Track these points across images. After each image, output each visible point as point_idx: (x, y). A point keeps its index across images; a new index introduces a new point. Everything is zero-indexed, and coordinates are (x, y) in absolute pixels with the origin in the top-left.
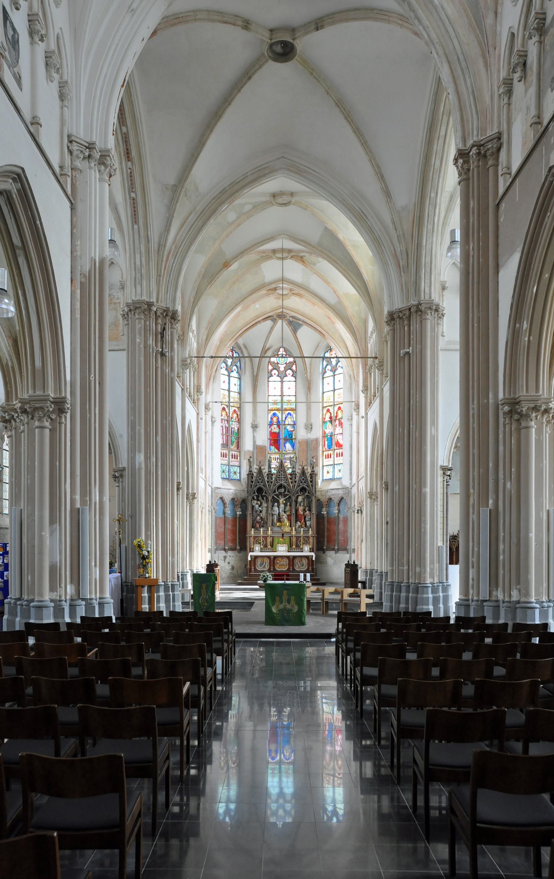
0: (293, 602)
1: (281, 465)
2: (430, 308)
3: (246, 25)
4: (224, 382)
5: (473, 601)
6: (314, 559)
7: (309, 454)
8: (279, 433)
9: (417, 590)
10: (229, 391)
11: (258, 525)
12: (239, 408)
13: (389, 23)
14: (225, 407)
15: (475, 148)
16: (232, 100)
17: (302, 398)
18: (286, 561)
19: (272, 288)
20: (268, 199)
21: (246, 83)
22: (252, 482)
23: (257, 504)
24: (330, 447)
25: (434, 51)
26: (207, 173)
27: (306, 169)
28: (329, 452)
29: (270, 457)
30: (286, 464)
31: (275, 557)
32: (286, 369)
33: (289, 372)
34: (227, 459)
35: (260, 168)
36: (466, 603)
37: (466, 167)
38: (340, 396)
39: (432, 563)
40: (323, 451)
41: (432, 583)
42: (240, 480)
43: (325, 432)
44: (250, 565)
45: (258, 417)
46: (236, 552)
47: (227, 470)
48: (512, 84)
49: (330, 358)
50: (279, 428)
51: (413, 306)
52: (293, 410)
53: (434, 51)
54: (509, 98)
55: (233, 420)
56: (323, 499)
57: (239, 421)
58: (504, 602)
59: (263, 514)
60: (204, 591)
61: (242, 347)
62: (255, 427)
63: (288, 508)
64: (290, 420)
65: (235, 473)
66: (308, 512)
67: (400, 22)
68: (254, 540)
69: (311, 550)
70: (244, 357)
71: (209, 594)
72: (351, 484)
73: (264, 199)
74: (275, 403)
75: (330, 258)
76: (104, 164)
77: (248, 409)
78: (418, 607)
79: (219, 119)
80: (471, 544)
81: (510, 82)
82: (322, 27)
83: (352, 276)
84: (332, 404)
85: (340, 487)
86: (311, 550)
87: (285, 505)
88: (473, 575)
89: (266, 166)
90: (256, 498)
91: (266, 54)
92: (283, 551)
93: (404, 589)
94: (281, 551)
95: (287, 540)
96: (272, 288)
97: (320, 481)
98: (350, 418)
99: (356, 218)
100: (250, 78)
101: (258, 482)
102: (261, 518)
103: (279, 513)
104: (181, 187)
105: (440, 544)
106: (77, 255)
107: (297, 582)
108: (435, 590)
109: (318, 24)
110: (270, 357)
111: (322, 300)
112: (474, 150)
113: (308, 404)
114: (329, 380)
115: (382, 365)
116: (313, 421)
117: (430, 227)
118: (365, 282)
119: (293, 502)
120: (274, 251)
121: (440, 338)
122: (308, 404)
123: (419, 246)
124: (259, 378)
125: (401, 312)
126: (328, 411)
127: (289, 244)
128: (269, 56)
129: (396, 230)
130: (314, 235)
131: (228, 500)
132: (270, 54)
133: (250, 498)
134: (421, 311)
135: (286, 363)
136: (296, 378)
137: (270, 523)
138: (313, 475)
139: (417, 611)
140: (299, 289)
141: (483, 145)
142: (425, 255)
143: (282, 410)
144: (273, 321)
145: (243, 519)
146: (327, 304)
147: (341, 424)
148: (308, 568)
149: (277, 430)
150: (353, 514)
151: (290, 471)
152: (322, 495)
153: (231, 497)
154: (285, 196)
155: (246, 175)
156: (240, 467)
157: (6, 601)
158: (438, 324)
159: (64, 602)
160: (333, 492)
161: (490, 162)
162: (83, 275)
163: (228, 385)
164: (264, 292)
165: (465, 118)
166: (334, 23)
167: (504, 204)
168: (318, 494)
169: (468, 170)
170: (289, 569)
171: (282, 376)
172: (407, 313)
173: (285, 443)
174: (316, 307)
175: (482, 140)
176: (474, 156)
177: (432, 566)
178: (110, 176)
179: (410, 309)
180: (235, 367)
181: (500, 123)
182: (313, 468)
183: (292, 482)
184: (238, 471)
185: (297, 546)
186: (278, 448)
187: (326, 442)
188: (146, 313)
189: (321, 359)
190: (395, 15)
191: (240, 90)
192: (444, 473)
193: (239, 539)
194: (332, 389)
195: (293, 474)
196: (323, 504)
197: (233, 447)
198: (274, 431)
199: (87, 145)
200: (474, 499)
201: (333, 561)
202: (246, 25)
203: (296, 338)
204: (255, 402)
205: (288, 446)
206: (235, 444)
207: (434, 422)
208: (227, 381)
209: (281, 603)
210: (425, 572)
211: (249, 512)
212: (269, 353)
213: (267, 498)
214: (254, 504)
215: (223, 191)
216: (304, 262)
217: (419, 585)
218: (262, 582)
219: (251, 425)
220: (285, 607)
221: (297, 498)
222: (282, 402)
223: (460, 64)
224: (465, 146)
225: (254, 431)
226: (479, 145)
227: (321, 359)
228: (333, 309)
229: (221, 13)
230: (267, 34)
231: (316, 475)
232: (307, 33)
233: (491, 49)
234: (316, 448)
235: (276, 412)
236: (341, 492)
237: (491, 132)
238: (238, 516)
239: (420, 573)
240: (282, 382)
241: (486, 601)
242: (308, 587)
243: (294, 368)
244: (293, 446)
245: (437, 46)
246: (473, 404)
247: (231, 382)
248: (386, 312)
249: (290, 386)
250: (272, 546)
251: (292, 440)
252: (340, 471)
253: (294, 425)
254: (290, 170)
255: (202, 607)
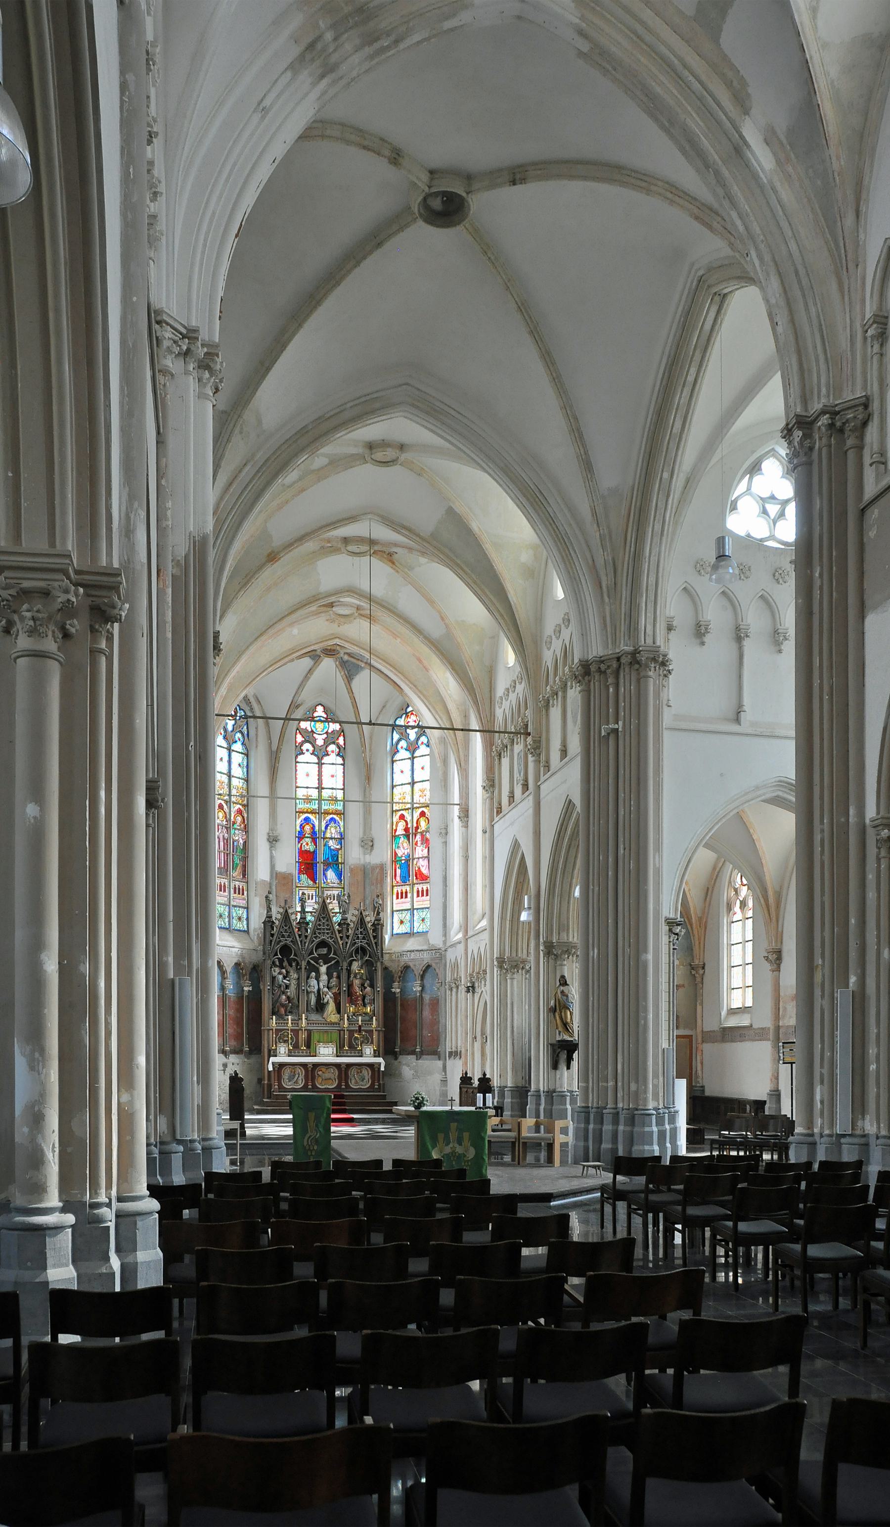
0: (466, 1142)
1: (324, 907)
2: (654, 660)
3: (396, 157)
4: (221, 759)
5: (822, 1136)
6: (382, 1069)
7: (367, 890)
8: (315, 852)
9: (632, 1120)
10: (230, 776)
11: (282, 1010)
12: (246, 806)
13: (648, 195)
14: (223, 802)
15: (827, 415)
16: (342, 278)
17: (355, 793)
18: (333, 1073)
19: (326, 603)
20: (360, 450)
21: (371, 252)
22: (272, 935)
23: (280, 973)
24: (405, 880)
25: (753, 253)
26: (277, 400)
27: (446, 408)
28: (404, 889)
29: (303, 894)
30: (330, 907)
31: (316, 1066)
32: (327, 743)
33: (332, 747)
34: (226, 894)
35: (368, 398)
36: (810, 1139)
37: (807, 443)
38: (424, 793)
39: (655, 1076)
40: (393, 887)
41: (656, 1109)
42: (247, 932)
43: (396, 854)
44: (269, 1079)
45: (279, 823)
46: (242, 1056)
47: (227, 914)
48: (886, 324)
49: (407, 727)
50: (315, 844)
51: (627, 653)
52: (340, 814)
53: (753, 253)
54: (882, 345)
55: (235, 826)
56: (394, 968)
57: (246, 829)
58: (878, 1138)
59: (292, 991)
60: (311, 1124)
61: (252, 700)
62: (273, 840)
63: (334, 981)
64: (333, 830)
65: (240, 919)
66: (368, 989)
67: (670, 195)
68: (277, 1035)
69: (376, 1054)
70: (255, 717)
71: (321, 1130)
72: (445, 942)
73: (353, 450)
74: (308, 800)
75: (452, 560)
76: (208, 367)
77: (261, 808)
78: (635, 1148)
79: (315, 307)
80: (818, 1047)
81: (883, 320)
82: (523, 181)
83: (488, 593)
84: (409, 806)
85: (425, 948)
86: (376, 1054)
87: (329, 975)
88: (822, 1095)
89: (375, 395)
90: (277, 963)
91: (416, 211)
92: (328, 1055)
93: (608, 1119)
94: (324, 1055)
95: (335, 1036)
96: (326, 603)
97: (387, 937)
98: (443, 831)
99: (528, 499)
100: (379, 245)
101: (283, 936)
102: (288, 998)
103: (319, 990)
104: (236, 417)
105: (665, 1045)
106: (168, 526)
107: (473, 1109)
108: (660, 1122)
109: (517, 175)
110: (300, 720)
111: (417, 629)
112: (825, 420)
113: (367, 803)
114: (402, 766)
115: (538, 747)
116: (375, 833)
117: (658, 527)
118: (511, 606)
119: (344, 971)
120: (346, 540)
121: (665, 708)
122: (367, 803)
123: (637, 557)
124: (283, 755)
125: (602, 662)
126: (402, 817)
127: (382, 533)
128: (421, 215)
129: (599, 527)
130: (427, 518)
131: (229, 967)
132: (422, 211)
133: (269, 962)
134: (638, 663)
135: (327, 733)
136: (344, 760)
137: (303, 1006)
138: (378, 926)
139: (634, 1156)
140: (372, 606)
141: (839, 413)
142: (648, 571)
143: (318, 813)
144: (313, 659)
145: (255, 999)
146: (426, 637)
147: (426, 841)
148: (373, 1084)
149: (311, 847)
150: (448, 992)
151: (337, 919)
152: (392, 961)
153: (235, 960)
154: (389, 449)
155: (342, 408)
156: (247, 908)
157: (791, 1139)
158: (663, 686)
159: (153, 1147)
160: (413, 955)
161: (850, 442)
162: (177, 563)
163: (227, 764)
164: (314, 608)
165: (805, 366)
166: (540, 178)
167: (876, 511)
168: (386, 957)
169: (811, 449)
170: (339, 1085)
171: (320, 754)
172: (615, 664)
173: (325, 870)
174: (399, 640)
175: (836, 405)
176: (823, 428)
177: (655, 1081)
178: (217, 390)
179: (618, 659)
180: (239, 735)
181: (865, 381)
182: (378, 914)
183: (341, 938)
184: (245, 916)
185: (351, 1047)
186: (313, 877)
187: (398, 871)
188: (75, 626)
189: (390, 728)
190: (660, 183)
191: (358, 263)
192: (670, 930)
193: (248, 1033)
194: (410, 780)
195: (343, 923)
196: (393, 976)
197: (237, 874)
198: (307, 848)
199: (184, 331)
200: (823, 976)
201: (412, 1072)
202: (396, 157)
203: (351, 691)
204: (273, 797)
205: (331, 874)
206: (239, 869)
207: (658, 848)
208: (226, 758)
209: (447, 1144)
210: (645, 1091)
211: (266, 986)
212: (298, 714)
213: (298, 964)
214: (275, 974)
215: (303, 431)
216: (393, 563)
217: (636, 1112)
218: (413, 1109)
219: (266, 837)
220: (454, 1151)
221: (350, 964)
222: (320, 799)
223: (799, 282)
224: (806, 410)
225: (271, 847)
226: (833, 412)
227: (390, 728)
228: (436, 647)
229: (361, 131)
230: (425, 177)
231: (382, 925)
232: (493, 186)
233: (851, 265)
234: (381, 881)
235: (310, 816)
236: (426, 957)
237: (852, 393)
238: (246, 994)
239: (637, 1093)
240: (320, 764)
241: (844, 1136)
242: (490, 1117)
243: (341, 741)
244: (339, 875)
245: (762, 246)
246: (822, 822)
247: (232, 760)
248: (576, 661)
249: (334, 773)
250: (308, 1046)
251: (337, 864)
252: (423, 920)
253: (341, 839)
254: (417, 407)
255: (309, 1153)
